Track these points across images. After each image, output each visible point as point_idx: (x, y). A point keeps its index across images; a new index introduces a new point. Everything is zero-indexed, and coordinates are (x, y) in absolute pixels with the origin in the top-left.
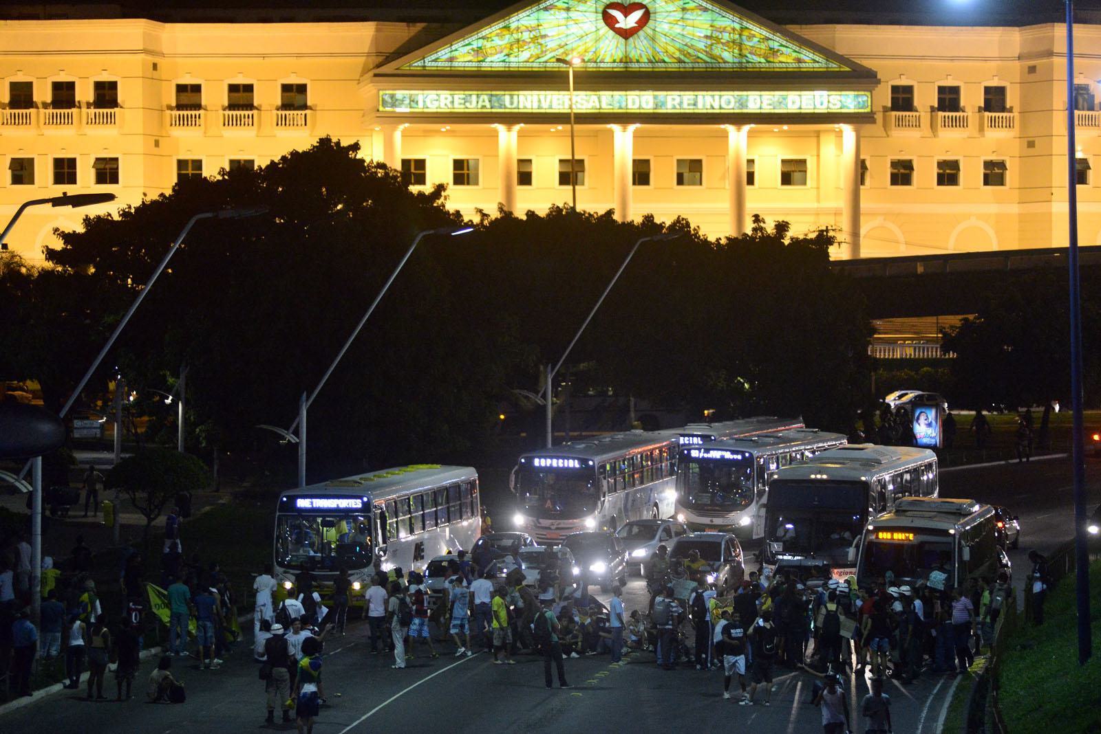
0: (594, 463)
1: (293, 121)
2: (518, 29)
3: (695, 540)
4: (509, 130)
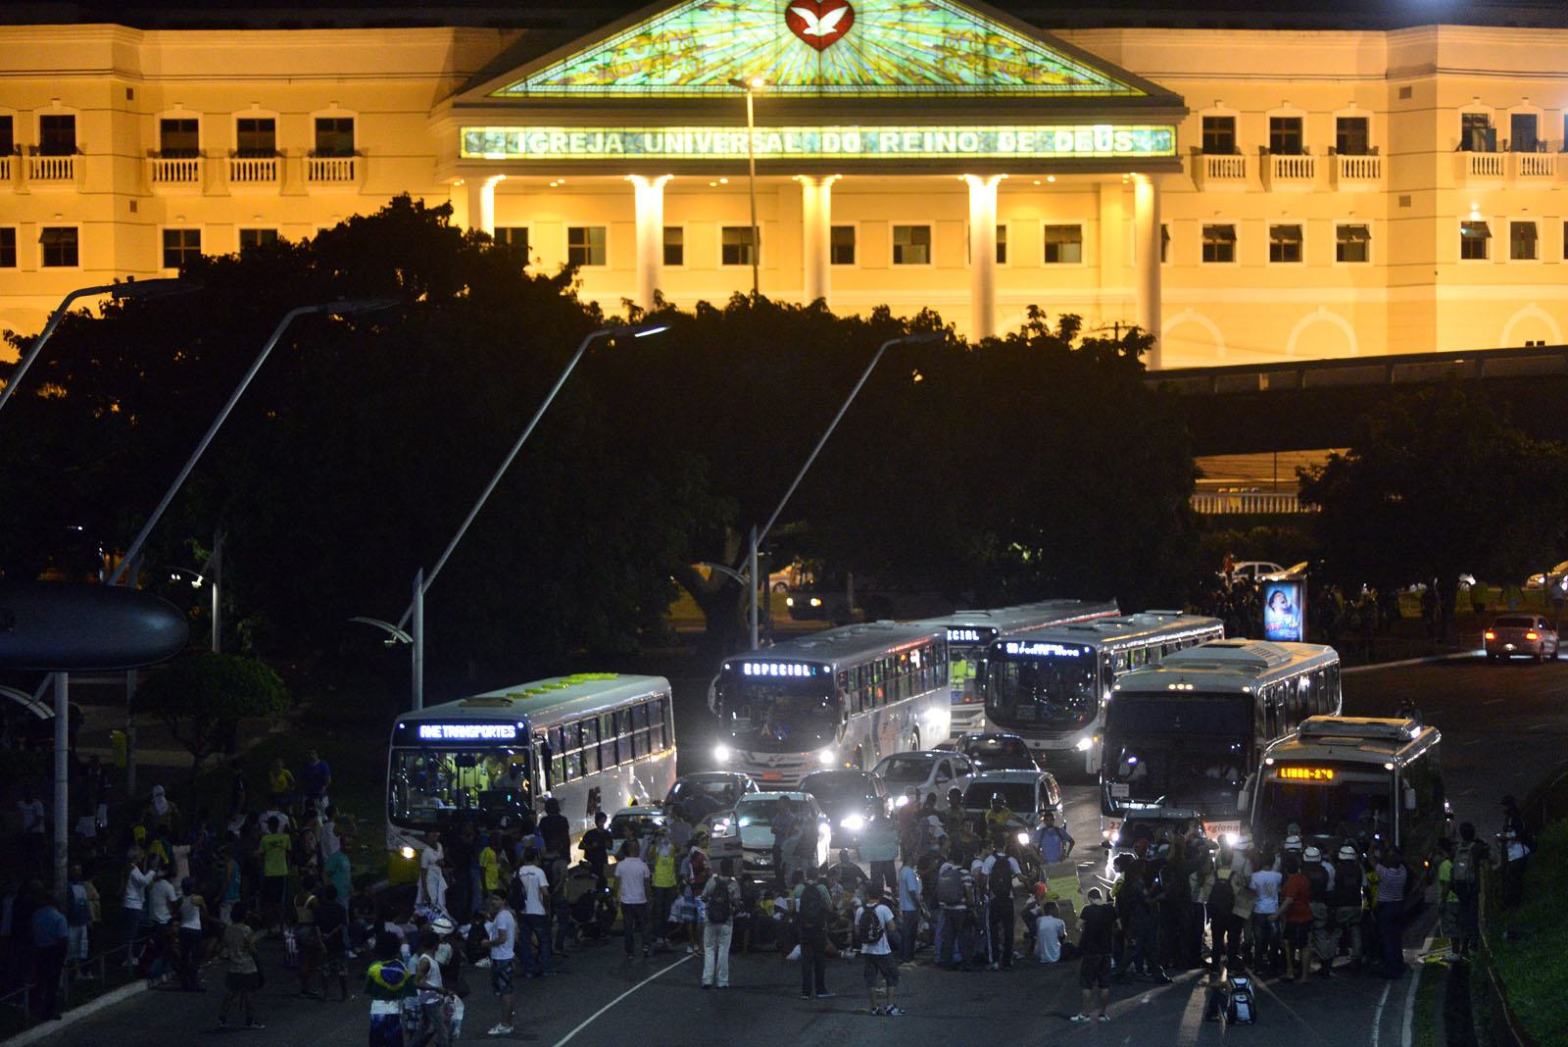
0: (831, 669)
1: (334, 172)
2: (663, 36)
3: (989, 781)
4: (819, 184)
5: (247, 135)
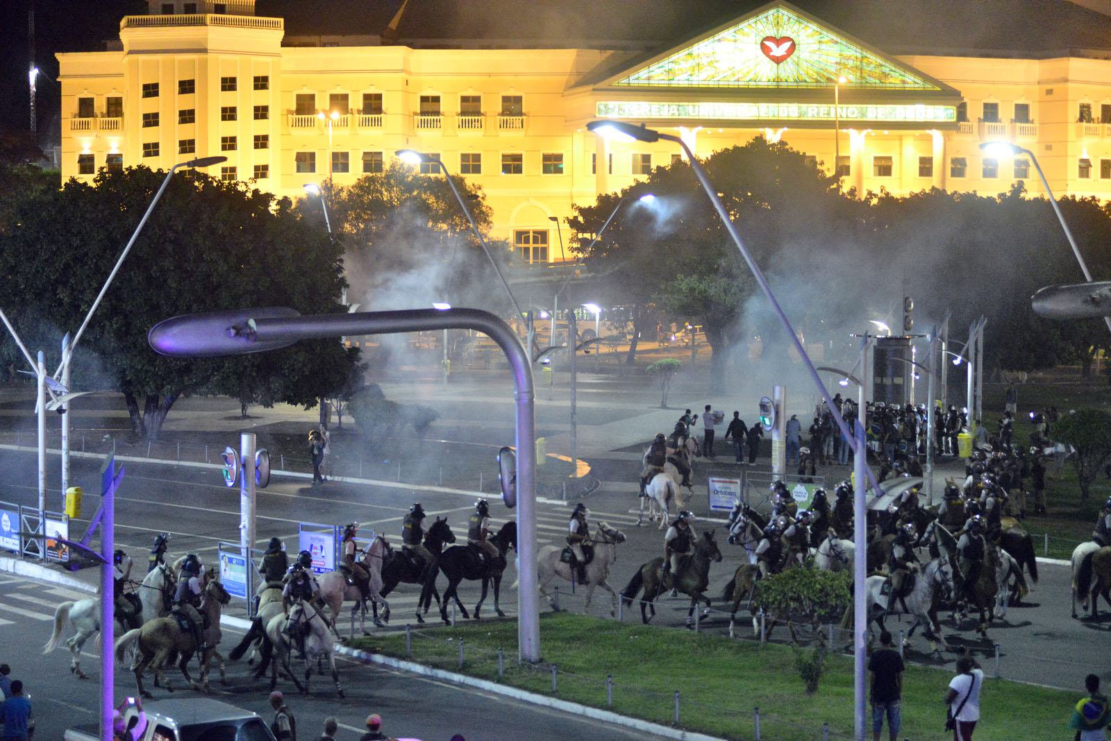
5: (465, 104)
